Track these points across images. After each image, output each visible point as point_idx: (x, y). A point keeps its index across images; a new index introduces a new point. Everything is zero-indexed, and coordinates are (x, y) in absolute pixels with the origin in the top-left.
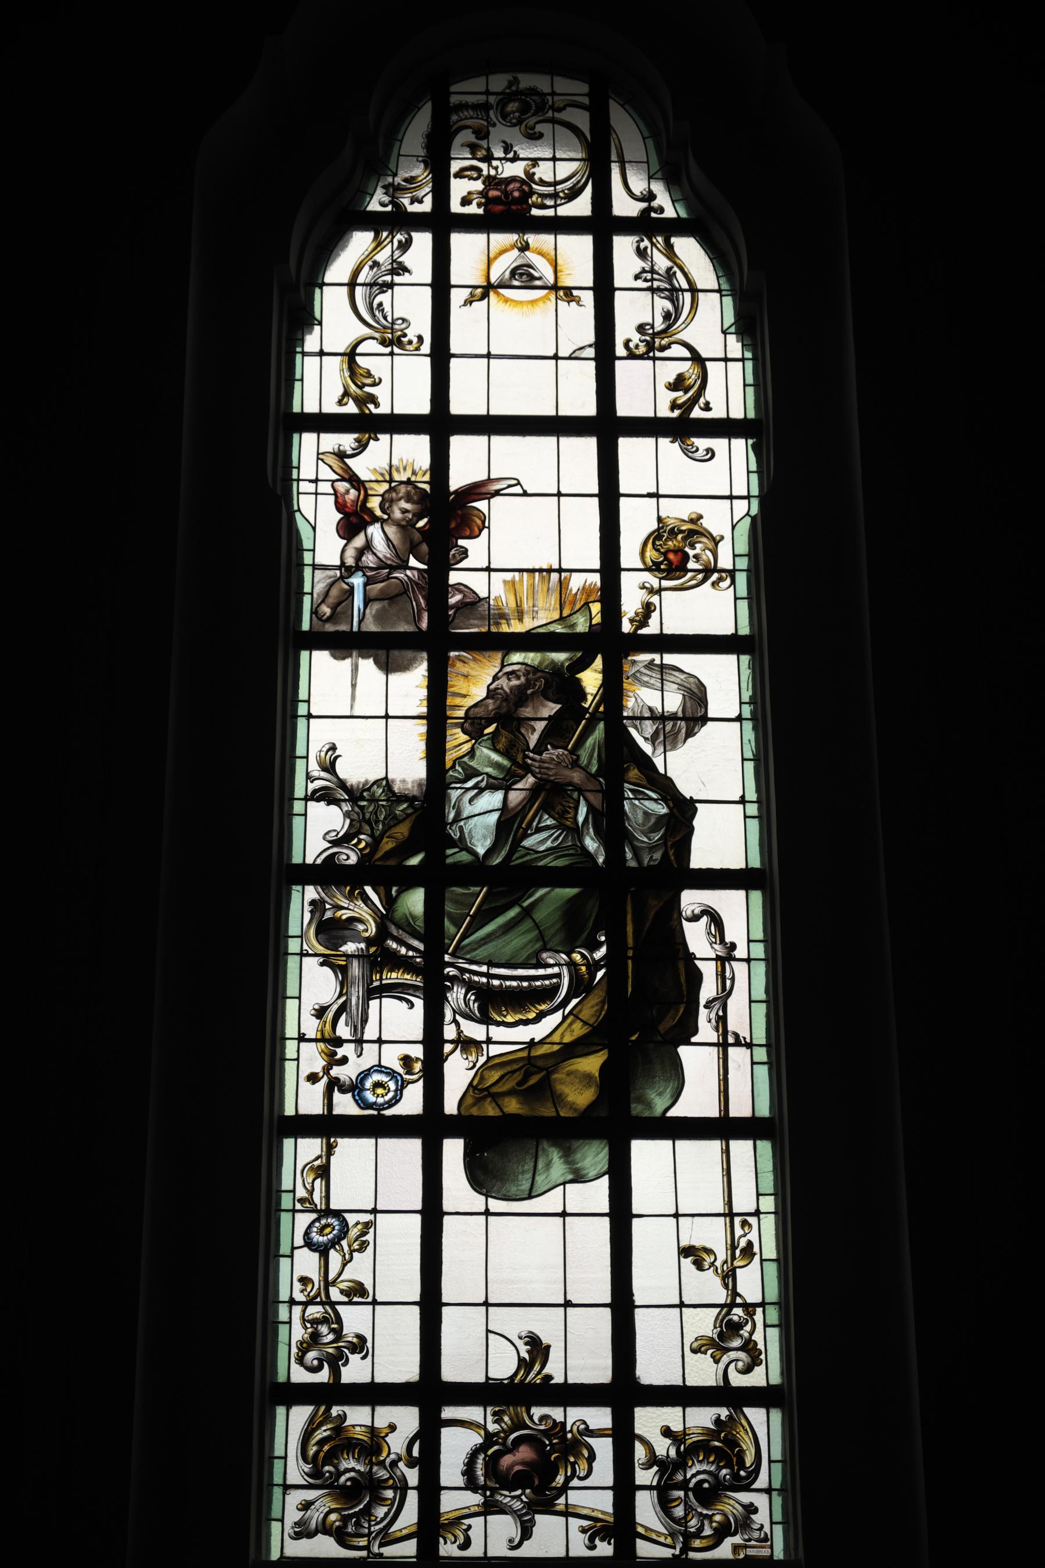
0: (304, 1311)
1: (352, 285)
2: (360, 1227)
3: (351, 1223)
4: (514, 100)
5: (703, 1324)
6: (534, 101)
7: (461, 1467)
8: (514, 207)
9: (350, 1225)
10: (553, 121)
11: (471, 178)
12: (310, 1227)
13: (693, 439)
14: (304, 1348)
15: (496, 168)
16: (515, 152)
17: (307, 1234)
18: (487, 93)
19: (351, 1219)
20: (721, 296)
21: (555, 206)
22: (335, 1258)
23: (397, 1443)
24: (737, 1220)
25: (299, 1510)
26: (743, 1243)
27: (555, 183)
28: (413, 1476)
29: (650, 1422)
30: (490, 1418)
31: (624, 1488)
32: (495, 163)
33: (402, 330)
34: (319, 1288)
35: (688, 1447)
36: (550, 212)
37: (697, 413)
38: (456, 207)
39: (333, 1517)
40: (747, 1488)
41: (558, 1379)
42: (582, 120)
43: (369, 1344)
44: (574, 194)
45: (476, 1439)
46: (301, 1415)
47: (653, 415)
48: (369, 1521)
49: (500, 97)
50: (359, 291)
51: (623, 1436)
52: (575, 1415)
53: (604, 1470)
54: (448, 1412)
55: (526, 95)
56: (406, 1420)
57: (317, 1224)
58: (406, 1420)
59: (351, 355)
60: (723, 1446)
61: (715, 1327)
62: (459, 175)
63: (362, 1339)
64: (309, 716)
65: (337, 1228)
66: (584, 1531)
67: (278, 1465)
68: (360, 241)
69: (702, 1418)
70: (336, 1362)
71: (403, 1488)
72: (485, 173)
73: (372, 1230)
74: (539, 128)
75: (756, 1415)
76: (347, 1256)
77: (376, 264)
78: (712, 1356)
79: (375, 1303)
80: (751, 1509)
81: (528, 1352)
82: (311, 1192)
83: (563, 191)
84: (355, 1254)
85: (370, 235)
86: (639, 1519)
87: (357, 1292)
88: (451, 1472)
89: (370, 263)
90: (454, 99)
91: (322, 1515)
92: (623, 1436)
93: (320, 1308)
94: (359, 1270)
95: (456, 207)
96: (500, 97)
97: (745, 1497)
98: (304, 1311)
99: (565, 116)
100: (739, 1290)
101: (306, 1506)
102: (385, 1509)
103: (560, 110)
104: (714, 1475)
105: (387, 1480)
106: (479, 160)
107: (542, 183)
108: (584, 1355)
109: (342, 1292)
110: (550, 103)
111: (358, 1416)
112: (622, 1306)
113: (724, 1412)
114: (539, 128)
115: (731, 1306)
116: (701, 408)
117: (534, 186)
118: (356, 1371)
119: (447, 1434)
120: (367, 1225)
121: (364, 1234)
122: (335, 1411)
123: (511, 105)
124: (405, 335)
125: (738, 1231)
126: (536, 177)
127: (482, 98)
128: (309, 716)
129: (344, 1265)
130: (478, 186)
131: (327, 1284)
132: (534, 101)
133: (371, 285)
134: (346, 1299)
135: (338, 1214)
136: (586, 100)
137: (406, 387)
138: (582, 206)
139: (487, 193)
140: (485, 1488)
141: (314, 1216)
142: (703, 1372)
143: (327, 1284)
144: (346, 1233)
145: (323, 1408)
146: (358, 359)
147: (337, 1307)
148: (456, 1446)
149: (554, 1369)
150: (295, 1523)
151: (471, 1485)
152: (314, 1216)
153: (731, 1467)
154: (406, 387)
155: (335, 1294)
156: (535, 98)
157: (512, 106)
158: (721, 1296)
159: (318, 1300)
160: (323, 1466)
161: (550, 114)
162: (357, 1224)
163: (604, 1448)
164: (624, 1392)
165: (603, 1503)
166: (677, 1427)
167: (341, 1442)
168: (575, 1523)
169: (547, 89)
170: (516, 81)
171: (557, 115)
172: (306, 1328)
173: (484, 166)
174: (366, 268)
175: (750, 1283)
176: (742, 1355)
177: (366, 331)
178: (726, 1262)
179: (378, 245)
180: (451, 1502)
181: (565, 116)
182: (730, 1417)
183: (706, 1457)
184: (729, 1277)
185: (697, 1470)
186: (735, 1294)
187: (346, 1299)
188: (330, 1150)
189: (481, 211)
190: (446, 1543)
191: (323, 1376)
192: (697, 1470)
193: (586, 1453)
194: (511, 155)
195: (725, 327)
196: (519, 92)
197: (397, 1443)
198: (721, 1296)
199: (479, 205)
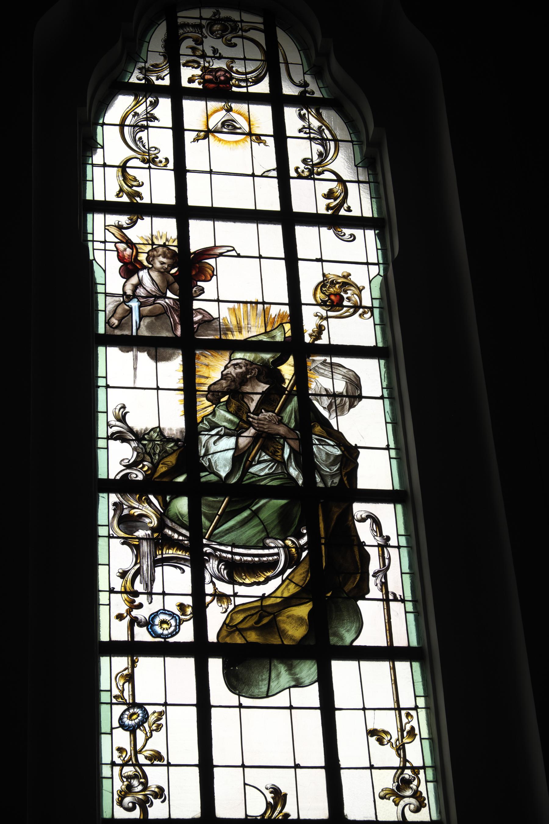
0: (121, 770)
1: (122, 125)
2: (156, 714)
5: (386, 780)
6: (230, 25)
8: (221, 86)
9: (150, 713)
10: (243, 37)
11: (193, 67)
12: (122, 714)
14: (123, 795)
15: (209, 62)
16: (220, 54)
17: (121, 719)
18: (201, 18)
19: (150, 709)
21: (247, 87)
22: (140, 735)
24: (403, 713)
27: (246, 74)
32: (208, 59)
36: (244, 90)
37: (342, 212)
41: (294, 816)
42: (261, 38)
43: (166, 792)
44: (258, 80)
47: (254, 208)
49: (208, 21)
55: (225, 21)
57: (127, 713)
59: (123, 167)
61: (394, 782)
63: (161, 789)
65: (141, 715)
70: (144, 804)
72: (202, 65)
73: (164, 717)
74: (234, 41)
76: (148, 734)
77: (136, 114)
81: (273, 798)
82: (122, 692)
83: (251, 78)
84: (154, 733)
85: (132, 98)
87: (156, 758)
89: (133, 113)
90: (180, 21)
93: (132, 768)
94: (157, 743)
96: (208, 21)
98: (121, 770)
103: (246, 31)
106: (198, 56)
107: (238, 72)
109: (146, 757)
110: (240, 27)
112: (332, 768)
114: (234, 41)
116: (345, 210)
117: (233, 74)
120: (161, 714)
121: (159, 719)
123: (216, 26)
124: (157, 157)
125: (405, 720)
127: (198, 21)
129: (147, 740)
131: (136, 753)
132: (230, 25)
134: (149, 762)
135: (141, 706)
136: (262, 26)
139: (204, 77)
141: (125, 707)
154: (160, 188)
155: (142, 759)
156: (230, 23)
157: (216, 27)
158: (396, 762)
159: (131, 763)
161: (240, 33)
162: (154, 712)
170: (218, 13)
171: (244, 34)
175: (416, 753)
176: (413, 800)
178: (398, 740)
179: (138, 103)
181: (252, 34)
184: (401, 750)
186: (405, 760)
187: (149, 762)
188: (133, 664)
189: (201, 87)
191: (136, 814)
194: (218, 55)
198: (396, 762)
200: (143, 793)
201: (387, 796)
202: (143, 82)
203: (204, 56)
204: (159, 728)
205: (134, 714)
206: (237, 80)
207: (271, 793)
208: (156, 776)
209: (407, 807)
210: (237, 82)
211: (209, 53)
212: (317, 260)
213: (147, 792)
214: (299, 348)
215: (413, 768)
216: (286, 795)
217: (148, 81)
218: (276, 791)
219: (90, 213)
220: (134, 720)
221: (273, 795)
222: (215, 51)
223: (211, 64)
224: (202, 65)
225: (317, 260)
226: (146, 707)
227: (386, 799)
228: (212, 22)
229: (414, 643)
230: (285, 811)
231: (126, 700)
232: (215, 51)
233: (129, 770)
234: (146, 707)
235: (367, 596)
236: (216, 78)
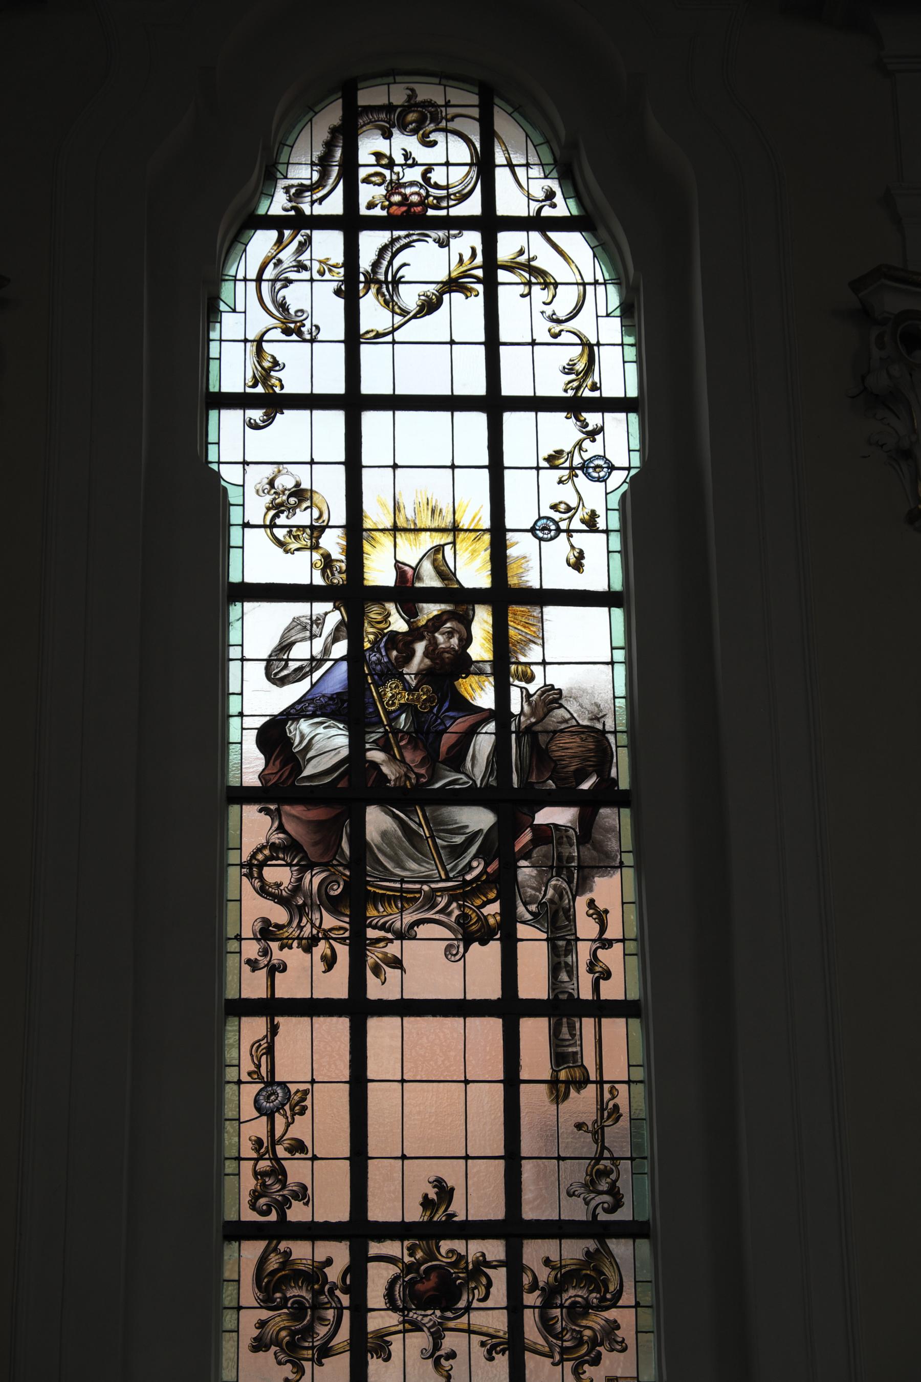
0: (255, 1165)
1: (259, 280)
2: (299, 1095)
3: (293, 1090)
4: (414, 111)
5: (576, 1173)
10: (446, 130)
11: (375, 184)
12: (258, 1094)
14: (256, 1196)
15: (398, 173)
16: (414, 159)
17: (256, 1101)
19: (293, 1088)
20: (235, 277)
21: (448, 207)
23: (333, 1274)
24: (606, 1087)
25: (257, 1328)
27: (447, 187)
28: (345, 1300)
31: (515, 1309)
33: (301, 321)
36: (443, 213)
37: (587, 393)
38: (363, 211)
40: (614, 1306)
41: (461, 1217)
43: (309, 1192)
44: (463, 197)
45: (392, 1270)
46: (252, 1250)
47: (450, 393)
50: (265, 286)
51: (514, 1264)
52: (474, 1248)
53: (499, 1294)
54: (375, 1248)
57: (264, 1093)
58: (339, 1254)
59: (260, 341)
60: (591, 1273)
61: (587, 1175)
62: (367, 180)
63: (304, 1188)
64: (243, 659)
65: (280, 1095)
68: (262, 242)
70: (282, 1206)
71: (340, 1310)
72: (388, 178)
73: (309, 1096)
74: (433, 137)
75: (620, 1248)
76: (290, 1120)
77: (280, 262)
79: (314, 1158)
80: (614, 1325)
81: (436, 1193)
82: (259, 1066)
83: (454, 194)
84: (297, 1117)
86: (526, 1336)
87: (298, 1147)
88: (375, 1296)
92: (514, 1264)
93: (268, 1163)
94: (300, 1129)
95: (363, 211)
97: (612, 1314)
98: (255, 1165)
99: (456, 125)
101: (262, 1324)
102: (326, 1329)
104: (586, 1299)
105: (327, 1303)
106: (382, 166)
107: (437, 186)
108: (482, 1199)
109: (286, 1149)
110: (444, 114)
111: (301, 1250)
112: (512, 1158)
115: (598, 1159)
117: (430, 189)
118: (297, 1213)
120: (306, 1092)
121: (304, 1100)
122: (283, 1245)
123: (411, 115)
124: (304, 325)
125: (607, 1096)
126: (432, 182)
128: (243, 659)
129: (288, 1125)
130: (382, 190)
131: (274, 1142)
133: (274, 281)
134: (289, 1156)
135: (283, 1084)
137: (315, 368)
138: (473, 207)
140: (402, 1310)
141: (262, 1085)
143: (274, 1142)
144: (289, 1099)
145: (275, 1242)
146: (264, 344)
148: (378, 1278)
150: (254, 1339)
152: (262, 1085)
153: (599, 1292)
154: (315, 368)
155: (281, 1152)
157: (411, 117)
159: (267, 1156)
160: (274, 1294)
161: (443, 124)
162: (298, 1091)
163: (499, 1277)
164: (513, 1229)
165: (498, 1322)
166: (554, 1257)
167: (291, 1273)
169: (441, 102)
172: (257, 1179)
173: (387, 173)
174: (271, 266)
176: (606, 1198)
177: (272, 322)
178: (596, 1121)
180: (375, 1322)
181: (456, 125)
185: (572, 1294)
188: (274, 1030)
190: (372, 1357)
191: (273, 1217)
192: (572, 1294)
194: (410, 162)
196: (417, 105)
197: (333, 1274)
198: (591, 1149)
203: (391, 165)
204: (302, 1112)
205: (273, 1094)
206: (435, 198)
207: (434, 1187)
210: (435, 201)
211: (399, 159)
214: (508, 596)
215: (612, 1159)
216: (452, 1189)
218: (439, 1183)
221: (436, 1190)
222: (407, 155)
223: (401, 176)
224: (388, 178)
226: (288, 1085)
228: (411, 105)
229: (617, 586)
230: (451, 1210)
232: (407, 155)
233: (264, 1165)
234: (288, 1085)
236: (405, 197)
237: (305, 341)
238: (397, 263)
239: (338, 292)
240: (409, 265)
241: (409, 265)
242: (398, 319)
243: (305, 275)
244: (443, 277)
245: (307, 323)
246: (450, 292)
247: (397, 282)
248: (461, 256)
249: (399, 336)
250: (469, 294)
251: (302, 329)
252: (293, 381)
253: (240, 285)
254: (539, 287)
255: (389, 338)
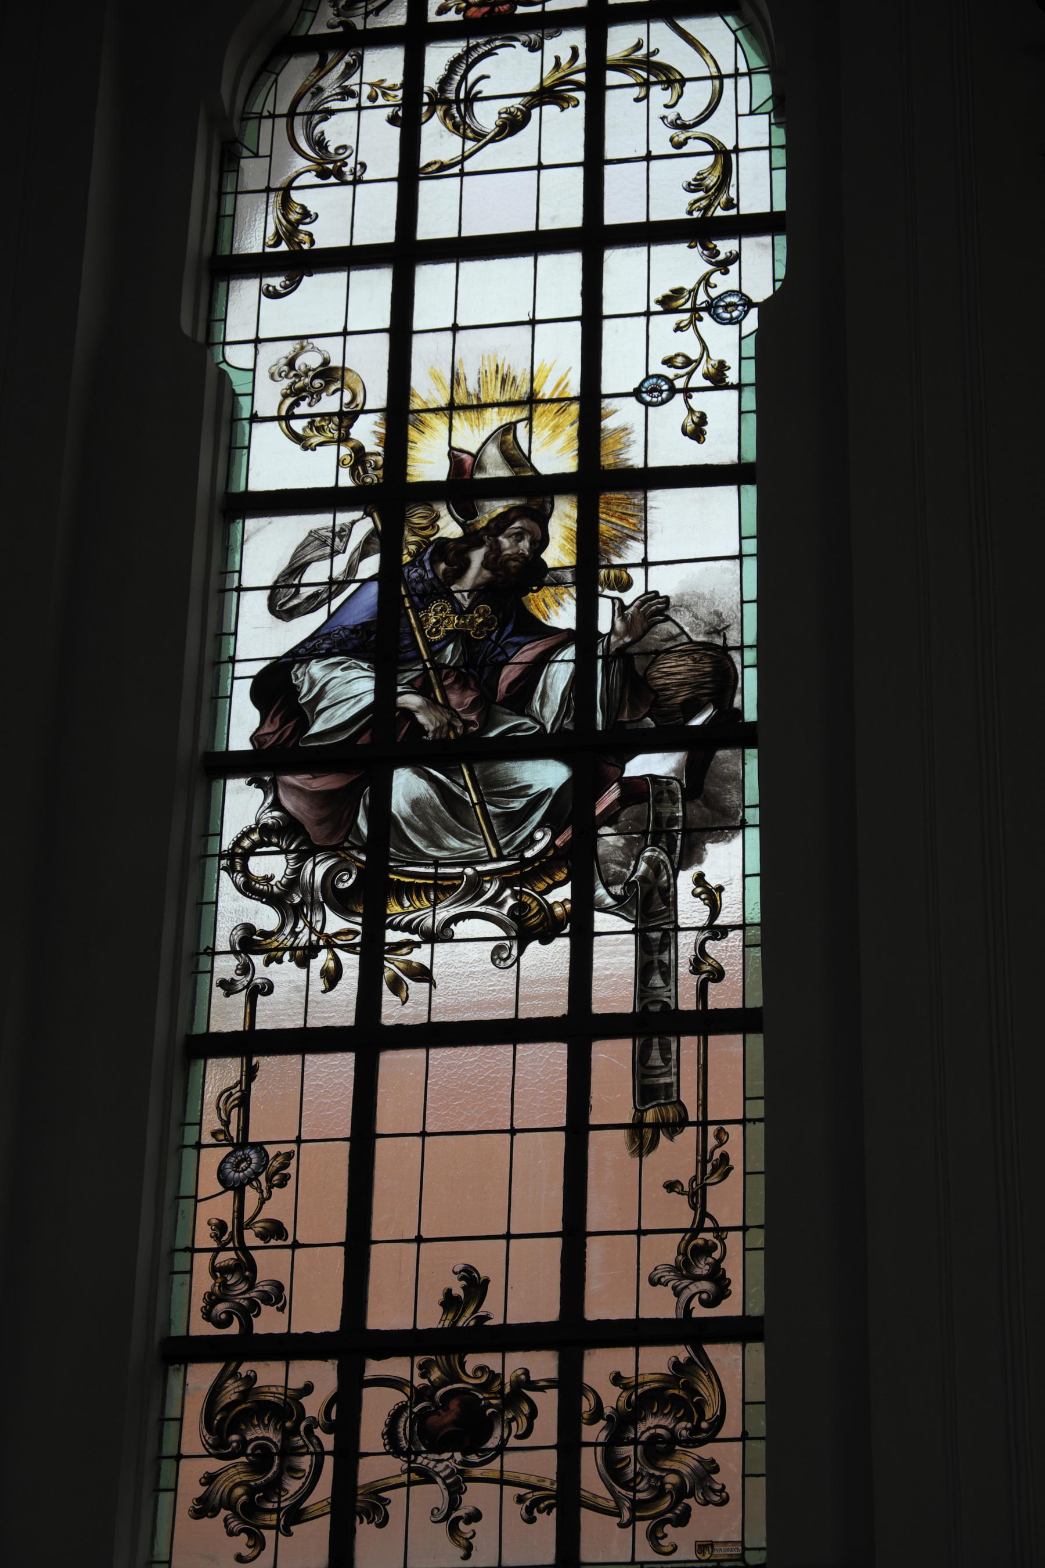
1: (291, 114)
2: (280, 1159)
5: (664, 1251)
7: (382, 1428)
9: (271, 1156)
12: (224, 1161)
13: (715, 242)
14: (212, 1300)
17: (221, 1171)
19: (271, 1150)
22: (251, 1195)
23: (313, 1406)
24: (712, 1130)
25: (202, 1484)
26: (717, 1155)
28: (328, 1441)
29: (600, 1367)
30: (416, 1371)
31: (568, 1447)
34: (232, 1232)
35: (643, 1399)
39: (239, 1491)
41: (496, 1320)
46: (202, 1377)
48: (280, 1496)
51: (570, 1384)
53: (547, 1426)
54: (374, 1368)
56: (322, 1377)
57: (232, 1160)
63: (280, 1287)
66: (520, 1499)
67: (171, 1428)
69: (657, 1361)
70: (247, 1313)
71: (319, 1457)
73: (294, 1162)
76: (265, 1194)
78: (674, 1288)
79: (296, 1245)
80: (711, 1467)
81: (464, 1288)
82: (227, 1123)
84: (275, 1190)
87: (275, 1230)
91: (227, 1490)
92: (570, 1384)
93: (232, 1254)
94: (278, 1206)
100: (709, 1210)
101: (210, 1479)
105: (301, 1447)
108: (529, 1293)
109: (257, 1235)
111: (270, 1375)
112: (574, 1233)
113: (682, 1353)
115: (696, 1230)
118: (268, 1322)
119: (369, 1395)
120: (289, 1156)
121: (285, 1165)
122: (245, 1369)
124: (346, 165)
125: (712, 1142)
129: (262, 1201)
131: (241, 1225)
134: (262, 1243)
135: (259, 1146)
142: (661, 1305)
145: (234, 1364)
147: (252, 1252)
148: (377, 1407)
149: (493, 1308)
150: (197, 1499)
151: (394, 1449)
155: (250, 1238)
158: (686, 1218)
159: (231, 1245)
162: (278, 1155)
163: (547, 1403)
164: (573, 1333)
165: (543, 1467)
166: (628, 1372)
167: (256, 1406)
168: (511, 1492)
172: (215, 1277)
175: (727, 1202)
178: (695, 1178)
179: (323, 69)
182: (690, 1360)
183: (661, 1408)
184: (697, 1197)
185: (651, 1425)
186: (704, 1214)
187: (262, 1243)
188: (251, 1073)
189: (460, 17)
191: (234, 1329)
192: (651, 1425)
193: (526, 1408)
195: (753, 108)
197: (313, 1406)
198: (686, 1218)
199: (458, 12)
200: (247, 1296)
201: (663, 1280)
202: (340, 29)
208: (270, 1264)
209: (697, 1297)
212: (647, 1232)
213: (253, 1294)
216: (487, 1281)
217: (349, 27)
219: (223, 281)
220: (243, 1171)
221: (464, 1283)
225: (647, 1232)
227: (662, 1284)
231: (232, 1138)
233: (226, 1257)
234: (266, 1147)
235: (683, 24)
237: (344, 183)
238: (472, 77)
239: (392, 120)
240: (488, 77)
241: (488, 77)
242: (470, 145)
243: (352, 103)
244: (532, 85)
245: (351, 162)
246: (541, 105)
247: (472, 98)
248: (557, 59)
249: (469, 166)
250: (565, 105)
251: (344, 169)
252: (327, 234)
253: (267, 124)
254: (659, 88)
255: (456, 170)
